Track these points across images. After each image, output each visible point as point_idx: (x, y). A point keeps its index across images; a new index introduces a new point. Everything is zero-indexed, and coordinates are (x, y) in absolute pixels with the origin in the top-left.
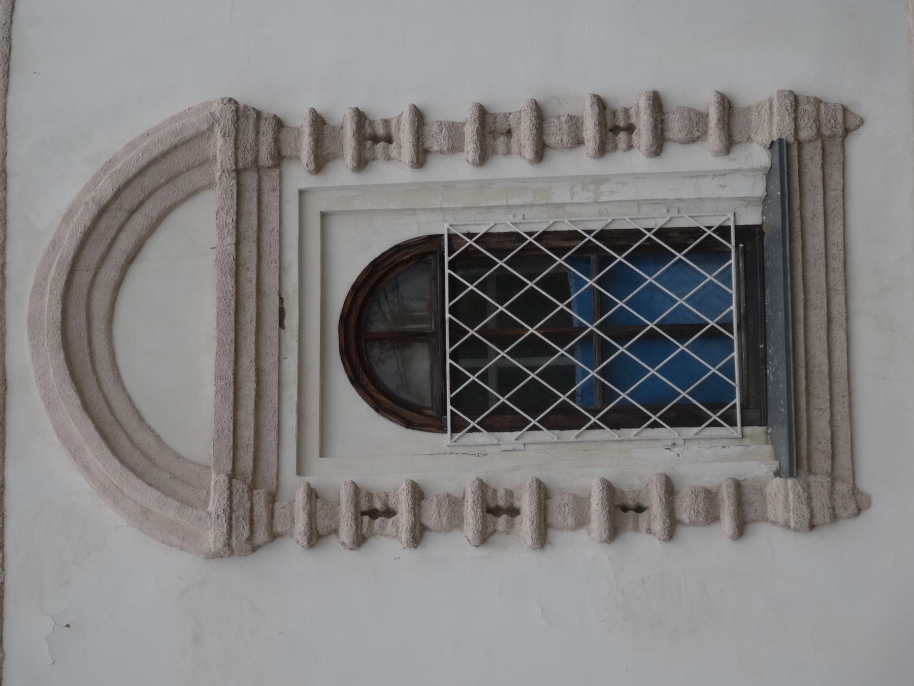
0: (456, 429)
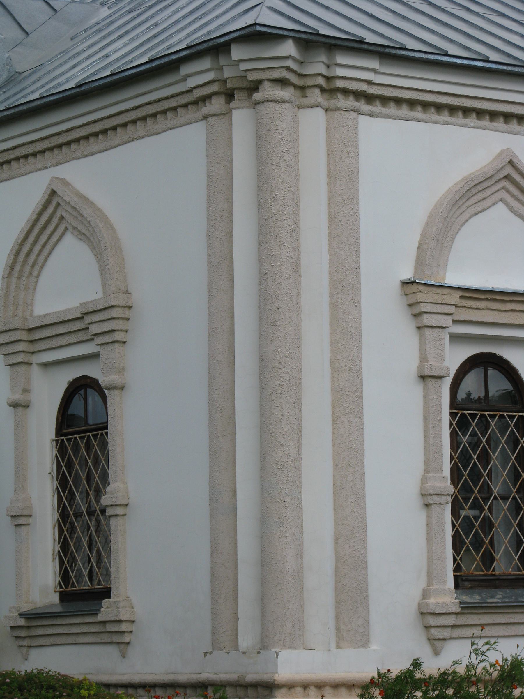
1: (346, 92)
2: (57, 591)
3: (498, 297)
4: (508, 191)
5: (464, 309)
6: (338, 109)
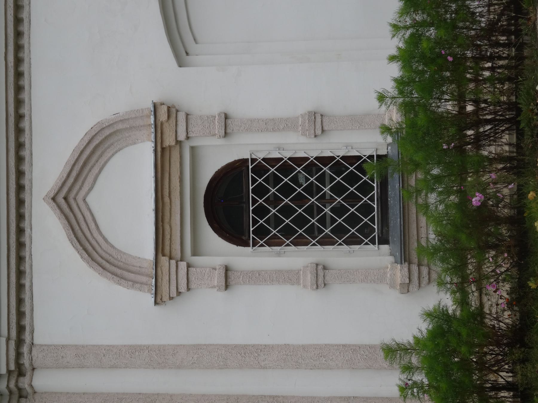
0: (254, 245)
1: (19, 355)
2: (378, 248)
3: (161, 236)
4: (77, 194)
5: (172, 246)
6: (31, 364)
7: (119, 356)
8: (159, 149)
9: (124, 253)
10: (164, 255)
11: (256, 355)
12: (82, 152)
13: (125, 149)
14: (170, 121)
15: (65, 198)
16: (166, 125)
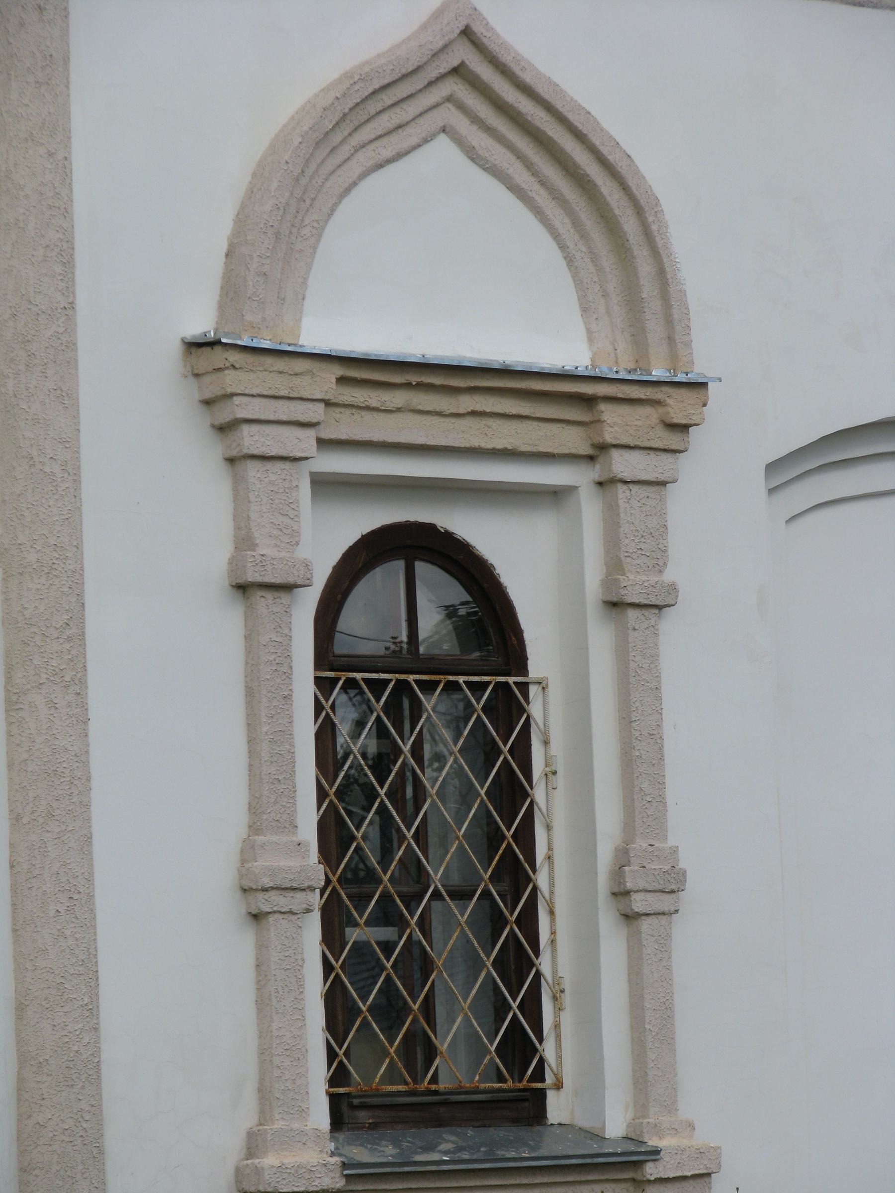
4: (461, 107)
7: (50, 207)
8: (588, 389)
9: (315, 248)
10: (341, 380)
11: (67, 678)
12: (579, 136)
13: (569, 275)
14: (661, 432)
15: (458, 71)
16: (650, 415)
